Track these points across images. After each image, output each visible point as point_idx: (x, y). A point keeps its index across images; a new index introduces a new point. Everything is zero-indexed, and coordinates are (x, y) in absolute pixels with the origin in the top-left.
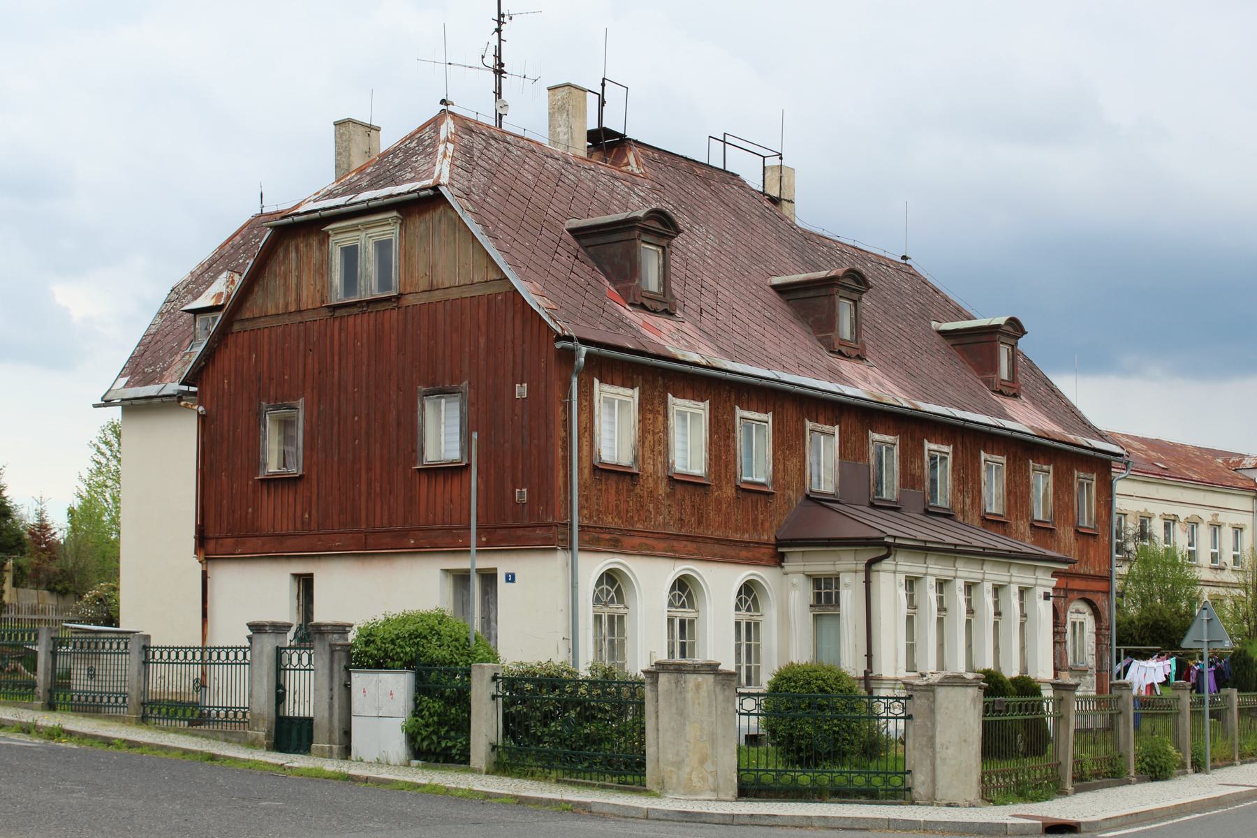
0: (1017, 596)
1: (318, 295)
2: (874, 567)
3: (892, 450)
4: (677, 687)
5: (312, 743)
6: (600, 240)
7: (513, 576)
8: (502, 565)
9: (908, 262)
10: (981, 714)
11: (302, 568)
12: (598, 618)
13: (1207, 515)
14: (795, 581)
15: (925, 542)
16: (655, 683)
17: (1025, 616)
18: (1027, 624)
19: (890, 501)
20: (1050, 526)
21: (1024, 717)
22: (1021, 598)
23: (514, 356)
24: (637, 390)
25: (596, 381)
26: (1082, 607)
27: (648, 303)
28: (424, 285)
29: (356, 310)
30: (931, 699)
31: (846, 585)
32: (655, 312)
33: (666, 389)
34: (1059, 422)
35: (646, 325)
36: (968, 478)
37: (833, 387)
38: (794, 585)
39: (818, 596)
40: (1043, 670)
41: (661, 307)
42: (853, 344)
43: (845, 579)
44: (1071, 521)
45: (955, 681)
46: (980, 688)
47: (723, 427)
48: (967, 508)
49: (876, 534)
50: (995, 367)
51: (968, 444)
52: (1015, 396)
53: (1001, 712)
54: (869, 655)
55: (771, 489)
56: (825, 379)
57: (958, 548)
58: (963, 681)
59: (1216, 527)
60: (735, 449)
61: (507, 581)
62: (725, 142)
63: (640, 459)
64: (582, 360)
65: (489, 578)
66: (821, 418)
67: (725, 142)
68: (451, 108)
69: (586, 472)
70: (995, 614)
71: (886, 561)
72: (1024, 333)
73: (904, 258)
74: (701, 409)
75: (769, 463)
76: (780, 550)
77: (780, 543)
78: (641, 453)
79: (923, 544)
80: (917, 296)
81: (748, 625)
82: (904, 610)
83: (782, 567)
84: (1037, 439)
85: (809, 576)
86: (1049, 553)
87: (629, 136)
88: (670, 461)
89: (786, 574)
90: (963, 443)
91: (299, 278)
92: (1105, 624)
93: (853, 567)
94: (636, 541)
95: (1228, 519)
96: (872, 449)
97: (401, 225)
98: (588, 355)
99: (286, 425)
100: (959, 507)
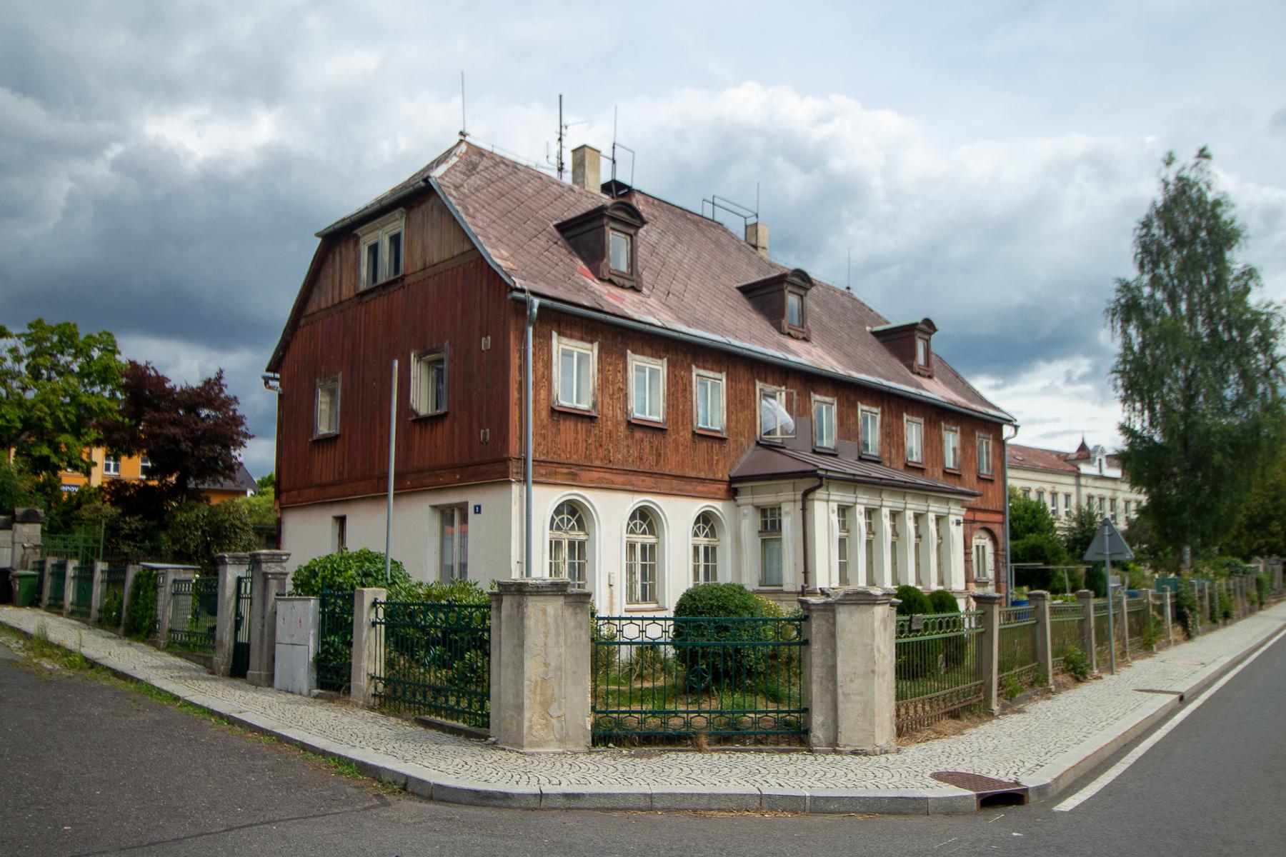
0: (934, 522)
1: (352, 287)
2: (810, 497)
3: (831, 408)
4: (518, 612)
5: (248, 669)
6: (578, 231)
7: (479, 507)
8: (472, 498)
9: (851, 291)
10: (895, 636)
11: (338, 511)
12: (556, 546)
13: (1048, 487)
14: (746, 511)
15: (854, 475)
16: (500, 601)
17: (941, 538)
18: (942, 545)
19: (829, 449)
20: (957, 472)
21: (945, 635)
22: (937, 524)
23: (482, 313)
24: (596, 345)
25: (555, 334)
26: (983, 534)
27: (615, 279)
28: (419, 265)
29: (374, 295)
30: (831, 620)
31: (787, 513)
32: (623, 287)
33: (626, 346)
34: (963, 396)
35: (610, 294)
36: (893, 436)
37: (779, 354)
38: (745, 515)
39: (765, 524)
40: (957, 583)
41: (628, 284)
42: (801, 329)
43: (786, 508)
44: (973, 469)
45: (864, 599)
46: (892, 605)
47: (680, 381)
48: (893, 457)
49: (810, 468)
50: (913, 355)
51: (893, 408)
52: (930, 377)
53: (918, 631)
54: (806, 572)
55: (725, 435)
56: (773, 349)
57: (883, 481)
58: (867, 597)
59: (1054, 495)
60: (692, 401)
61: (475, 512)
62: (713, 203)
63: (600, 405)
64: (535, 310)
65: (463, 508)
66: (770, 379)
67: (713, 203)
68: (468, 139)
69: (544, 414)
70: (916, 537)
71: (819, 491)
72: (935, 330)
73: (848, 288)
74: (660, 367)
75: (723, 414)
76: (734, 486)
77: (733, 480)
78: (600, 400)
79: (852, 477)
80: (856, 311)
81: (706, 549)
82: (837, 533)
83: (735, 500)
84: (949, 406)
85: (757, 507)
86: (959, 488)
87: (636, 186)
88: (629, 408)
89: (739, 506)
90: (888, 406)
91: (341, 277)
92: (1001, 547)
93: (792, 497)
94: (595, 475)
95: (1062, 490)
96: (814, 407)
97: (406, 219)
98: (541, 307)
99: (332, 393)
100: (887, 455)
